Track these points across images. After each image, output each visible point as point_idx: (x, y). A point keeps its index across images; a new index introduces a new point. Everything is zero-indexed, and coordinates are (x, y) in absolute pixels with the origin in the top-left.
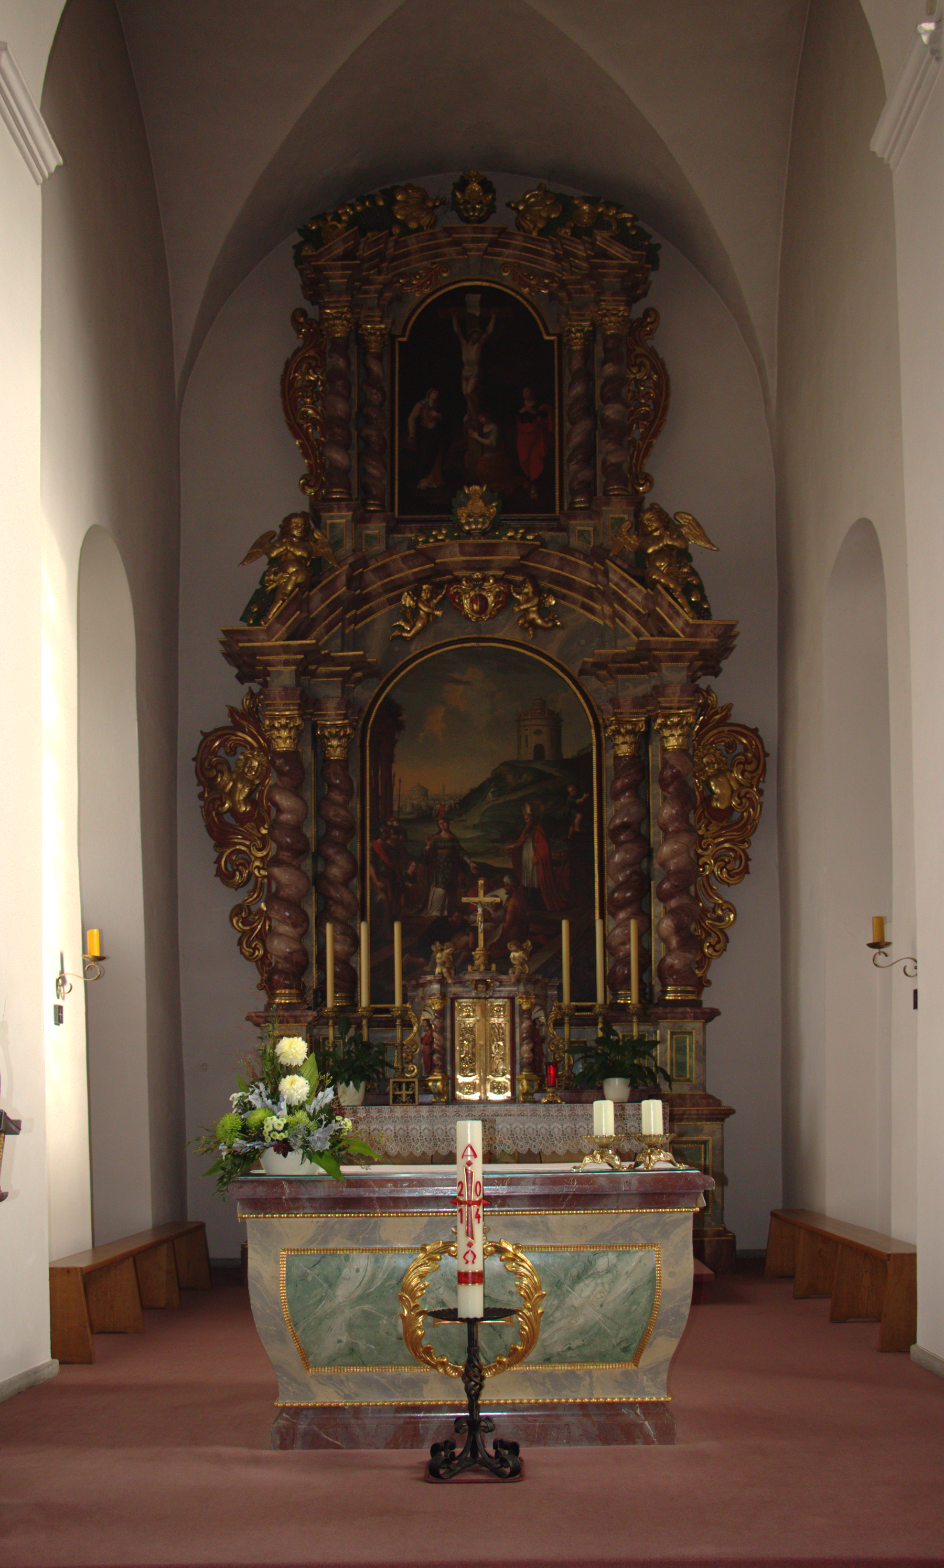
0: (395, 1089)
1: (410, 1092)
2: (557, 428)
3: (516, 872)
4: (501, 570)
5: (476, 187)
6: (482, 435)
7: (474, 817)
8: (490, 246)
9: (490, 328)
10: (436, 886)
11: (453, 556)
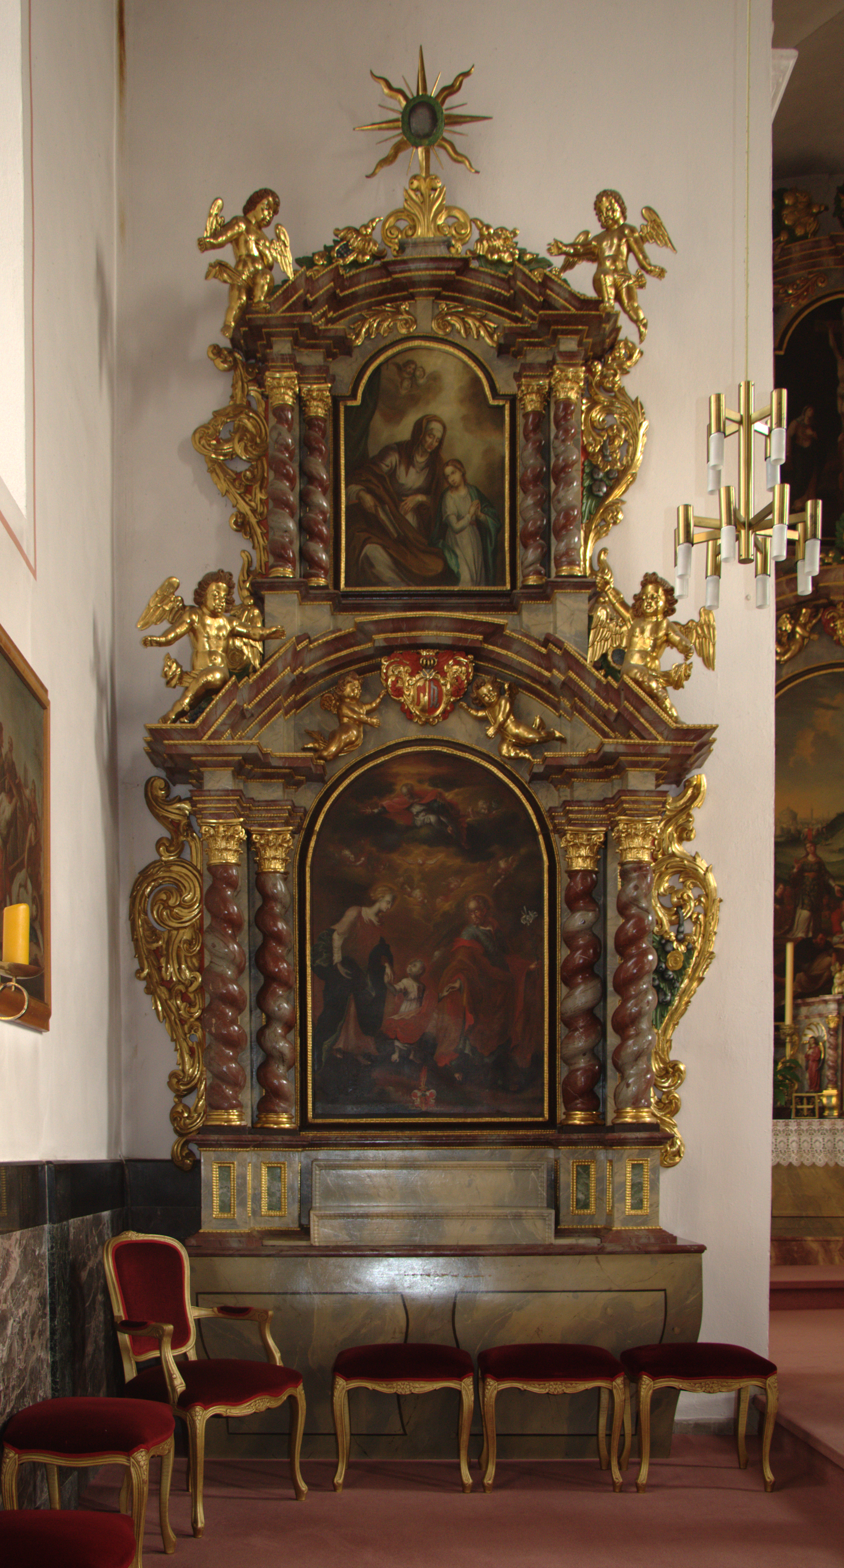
0: (797, 1104)
1: (811, 1106)
10: (802, 908)
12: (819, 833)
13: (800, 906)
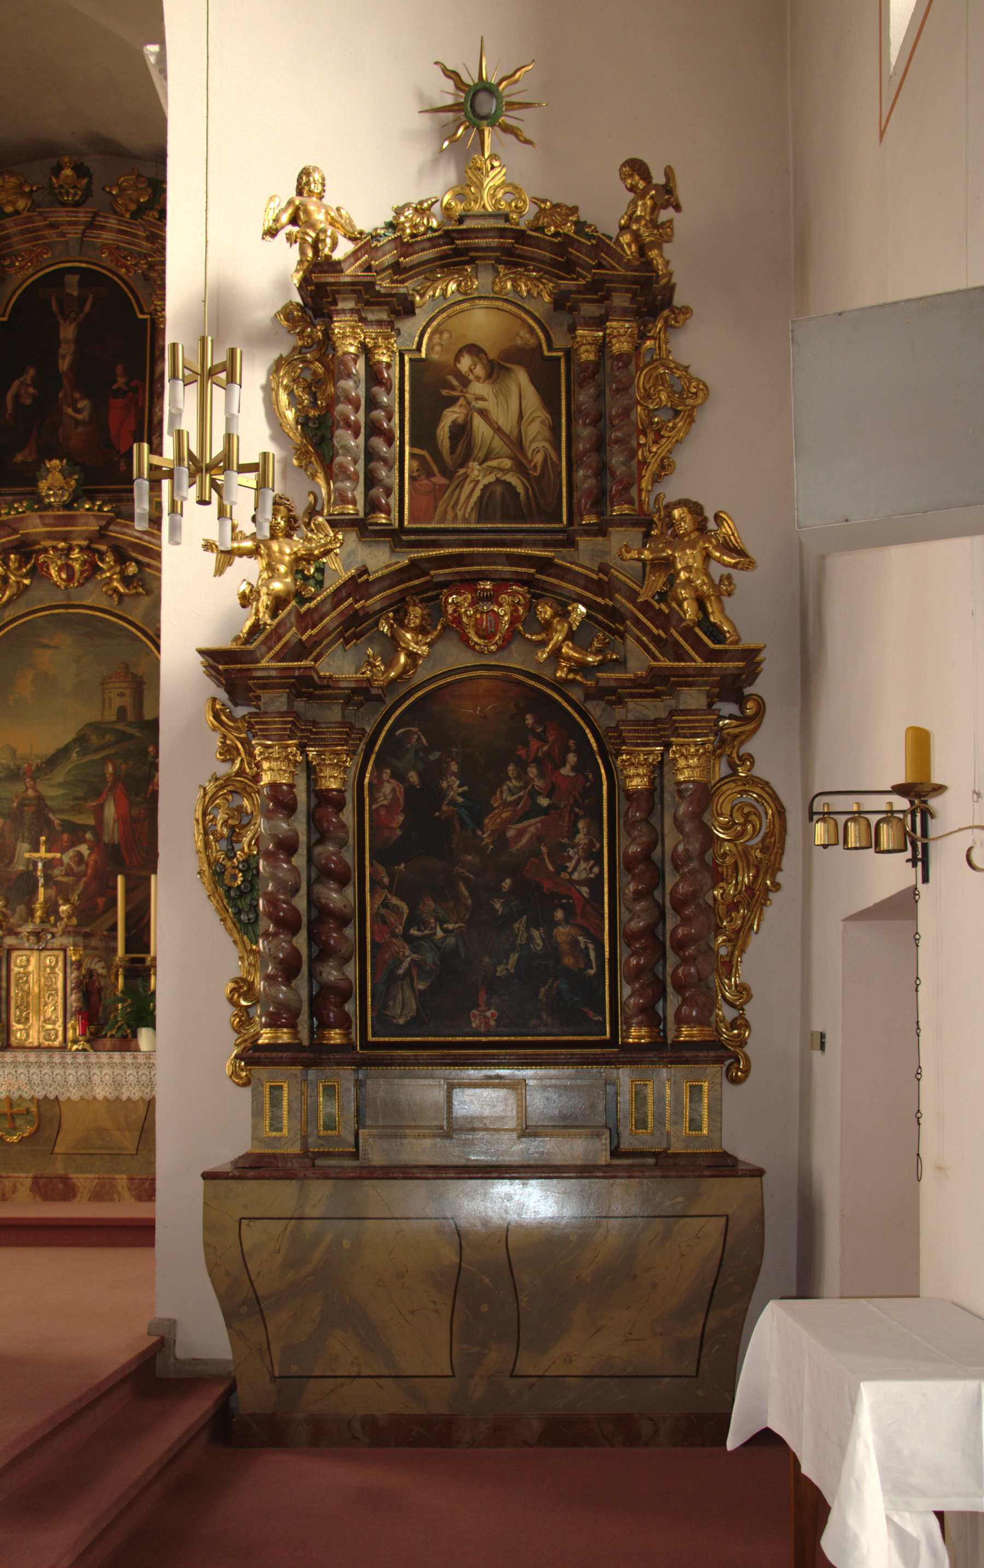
2: (147, 403)
3: (97, 830)
4: (85, 539)
5: (68, 172)
6: (77, 411)
7: (59, 775)
8: (87, 228)
9: (87, 308)
10: (23, 841)
11: (35, 526)
12: (39, 768)
13: (21, 839)
